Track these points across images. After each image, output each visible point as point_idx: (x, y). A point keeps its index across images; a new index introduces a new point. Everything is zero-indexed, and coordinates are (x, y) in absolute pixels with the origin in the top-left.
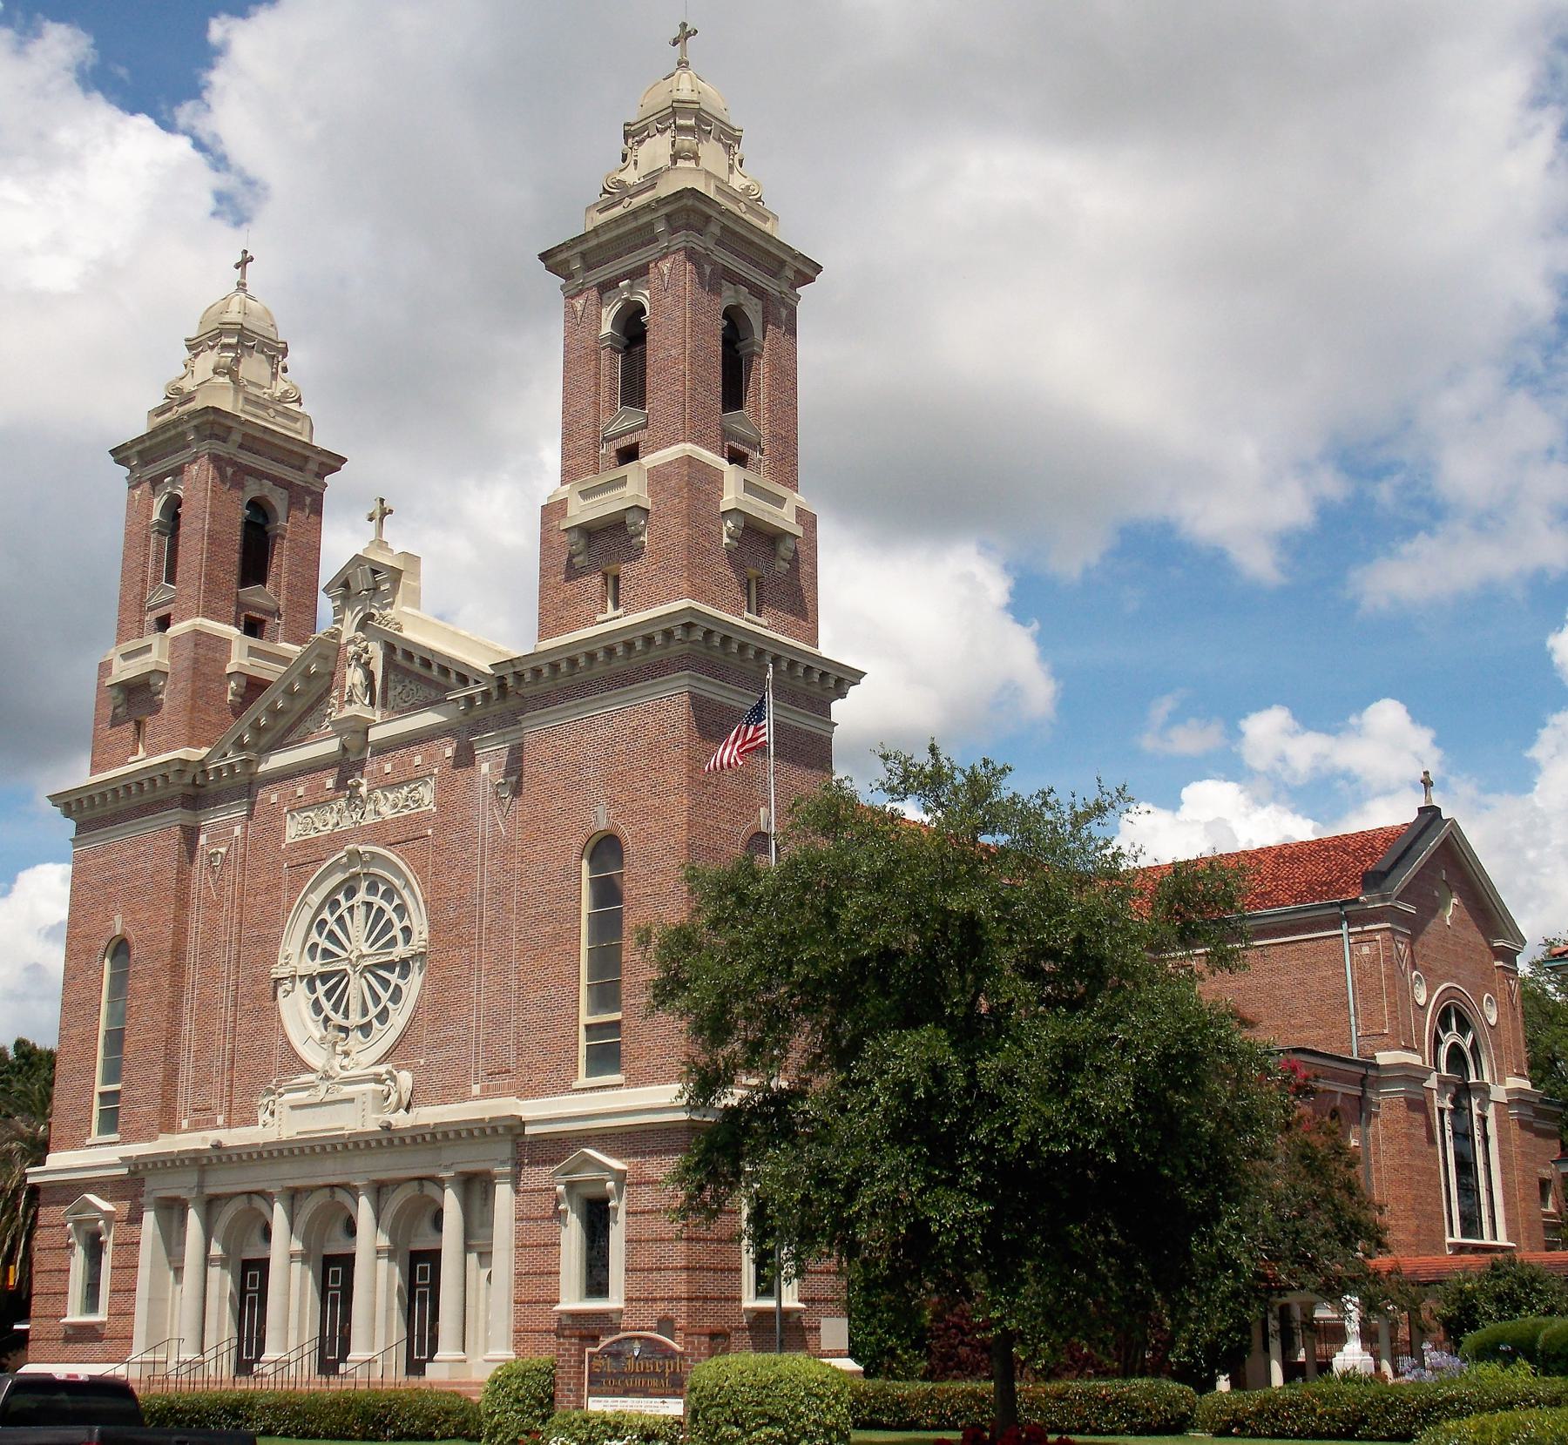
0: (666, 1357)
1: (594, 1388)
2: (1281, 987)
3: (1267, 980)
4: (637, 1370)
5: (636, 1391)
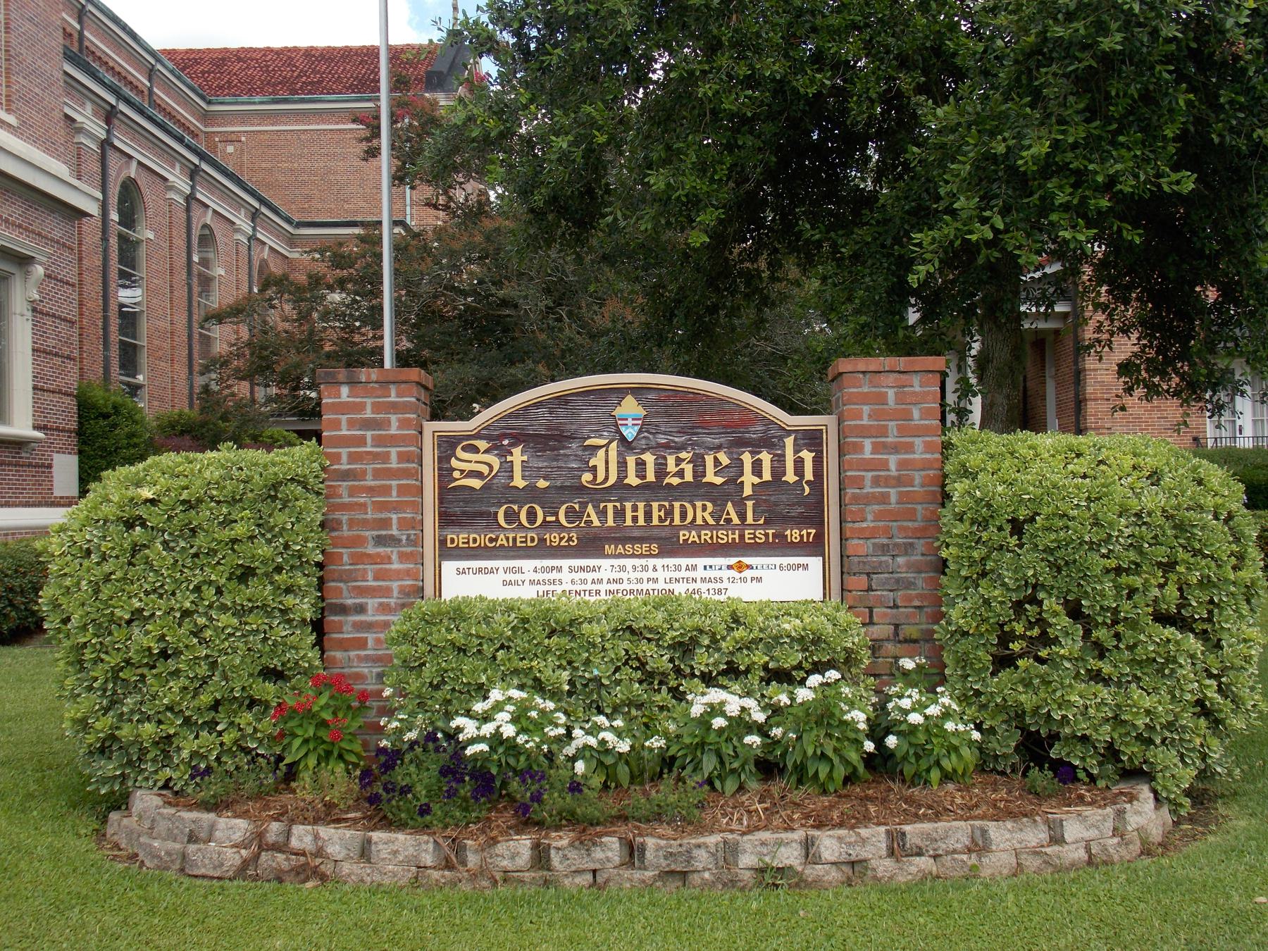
0: (742, 443)
1: (460, 537)
2: (335, 173)
3: (322, 164)
4: (632, 480)
5: (624, 540)
